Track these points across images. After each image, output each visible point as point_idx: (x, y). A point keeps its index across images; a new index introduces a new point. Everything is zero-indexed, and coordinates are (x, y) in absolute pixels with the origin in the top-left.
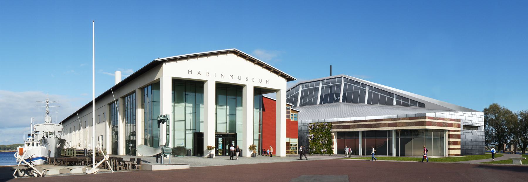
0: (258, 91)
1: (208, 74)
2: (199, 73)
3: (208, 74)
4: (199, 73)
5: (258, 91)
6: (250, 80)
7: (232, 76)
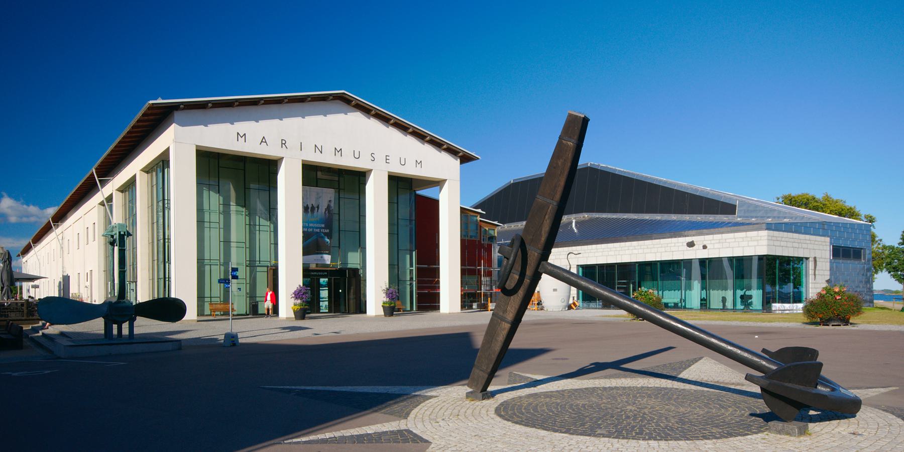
1: (283, 143)
3: (283, 143)
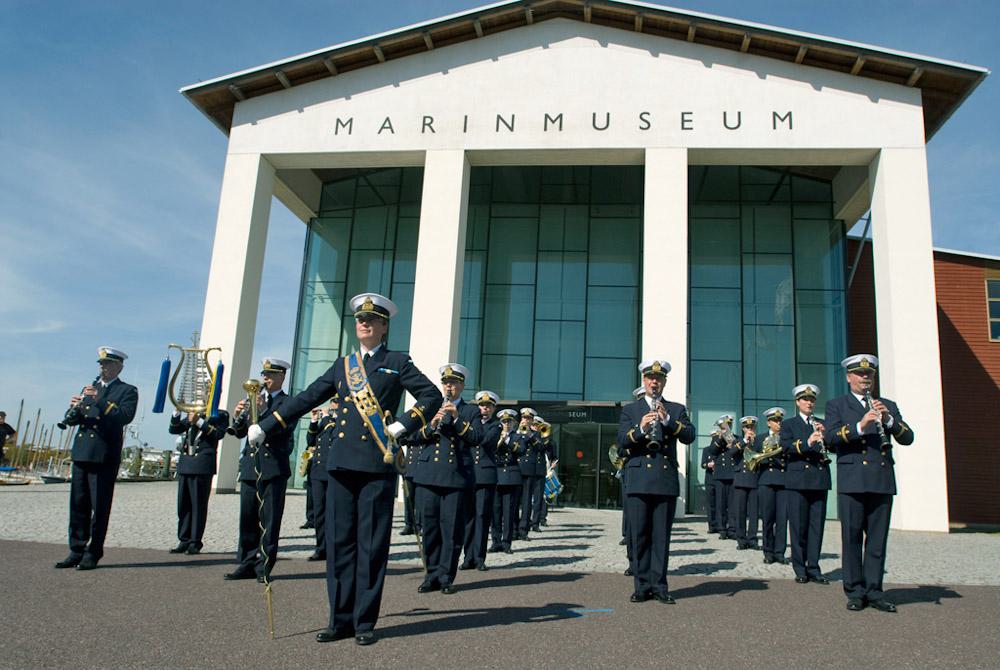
0: (717, 185)
1: (427, 123)
2: (387, 125)
3: (427, 123)
4: (387, 125)
5: (717, 185)
6: (665, 121)
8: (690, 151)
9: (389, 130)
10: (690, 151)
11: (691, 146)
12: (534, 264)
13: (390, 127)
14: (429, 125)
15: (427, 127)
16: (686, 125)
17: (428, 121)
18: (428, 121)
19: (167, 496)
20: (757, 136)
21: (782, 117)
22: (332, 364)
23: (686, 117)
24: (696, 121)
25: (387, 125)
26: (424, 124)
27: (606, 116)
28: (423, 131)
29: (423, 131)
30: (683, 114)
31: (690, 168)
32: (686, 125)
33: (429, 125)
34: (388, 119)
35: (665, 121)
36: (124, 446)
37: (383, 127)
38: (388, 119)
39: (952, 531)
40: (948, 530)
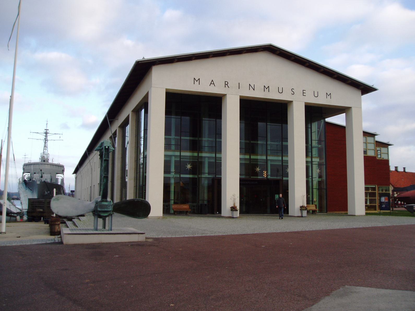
0: (314, 113)
1: (226, 84)
2: (212, 83)
3: (226, 84)
4: (212, 83)
6: (298, 92)
7: (266, 88)
8: (240, 96)
9: (213, 85)
10: (240, 96)
11: (305, 102)
12: (174, 144)
13: (214, 84)
14: (227, 85)
15: (226, 85)
16: (304, 94)
17: (226, 83)
18: (226, 83)
19: (380, 155)
20: (322, 100)
21: (329, 95)
22: (10, 209)
23: (304, 92)
24: (307, 93)
25: (212, 83)
26: (225, 84)
27: (331, 98)
28: (225, 87)
29: (225, 87)
30: (303, 90)
31: (166, 92)
32: (304, 94)
33: (227, 85)
34: (212, 81)
35: (298, 92)
36: (114, 213)
37: (211, 84)
38: (212, 81)
39: (367, 214)
40: (365, 214)
